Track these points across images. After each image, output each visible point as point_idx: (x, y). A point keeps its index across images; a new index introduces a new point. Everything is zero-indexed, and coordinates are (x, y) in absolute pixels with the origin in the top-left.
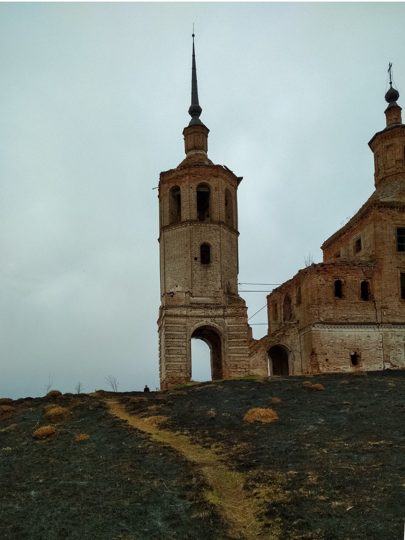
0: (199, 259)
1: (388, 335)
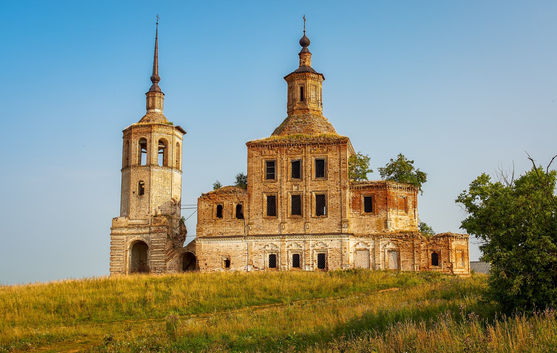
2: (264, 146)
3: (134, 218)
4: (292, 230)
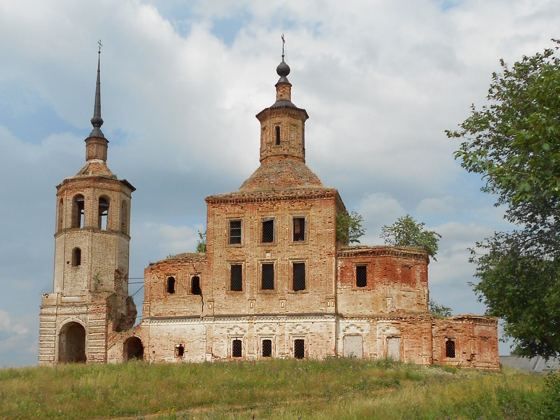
0: (70, 263)
1: (211, 328)
2: (227, 202)
3: (69, 294)
4: (263, 309)
